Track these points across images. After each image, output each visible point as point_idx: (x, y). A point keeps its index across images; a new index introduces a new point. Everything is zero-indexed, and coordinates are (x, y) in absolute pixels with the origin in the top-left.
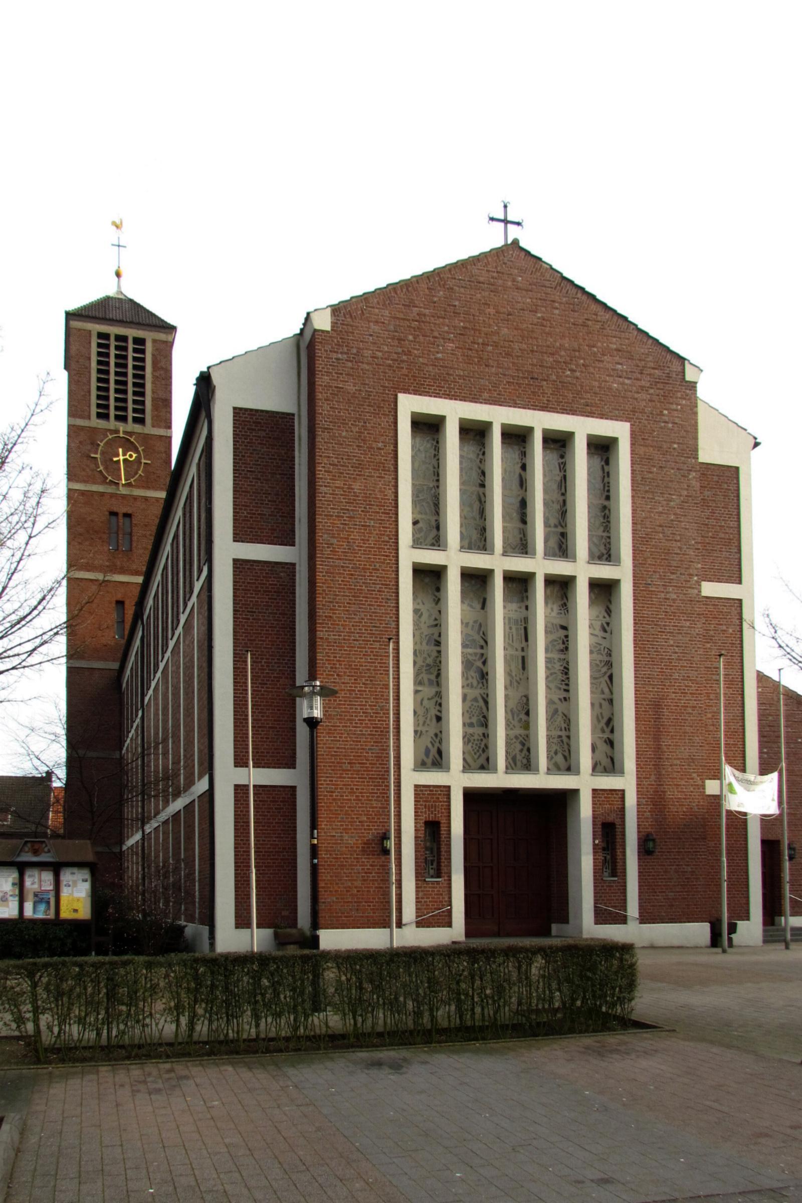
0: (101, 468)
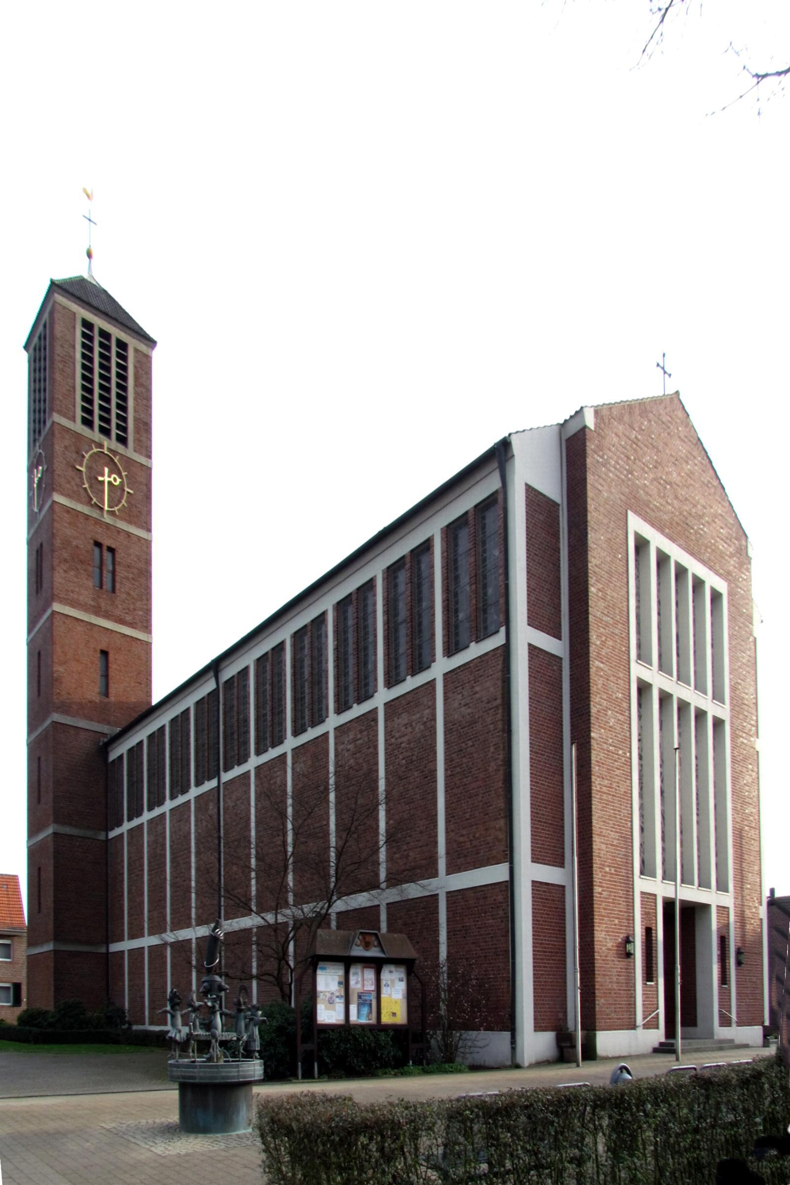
0: (86, 486)
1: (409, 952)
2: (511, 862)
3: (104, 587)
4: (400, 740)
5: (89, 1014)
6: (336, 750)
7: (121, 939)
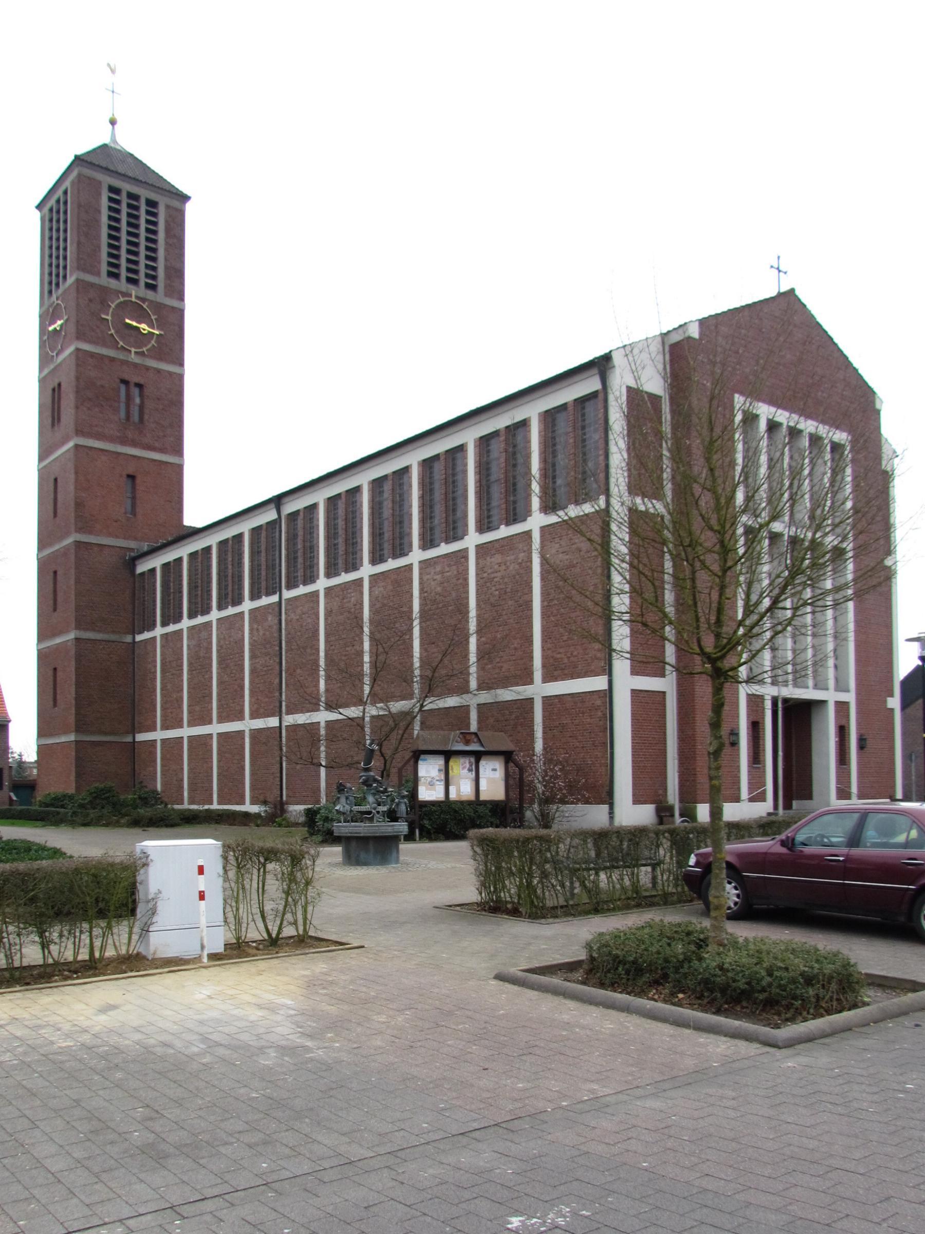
1: (507, 745)
2: (610, 675)
3: (131, 420)
4: (493, 576)
5: (122, 797)
6: (421, 579)
7: (153, 728)
